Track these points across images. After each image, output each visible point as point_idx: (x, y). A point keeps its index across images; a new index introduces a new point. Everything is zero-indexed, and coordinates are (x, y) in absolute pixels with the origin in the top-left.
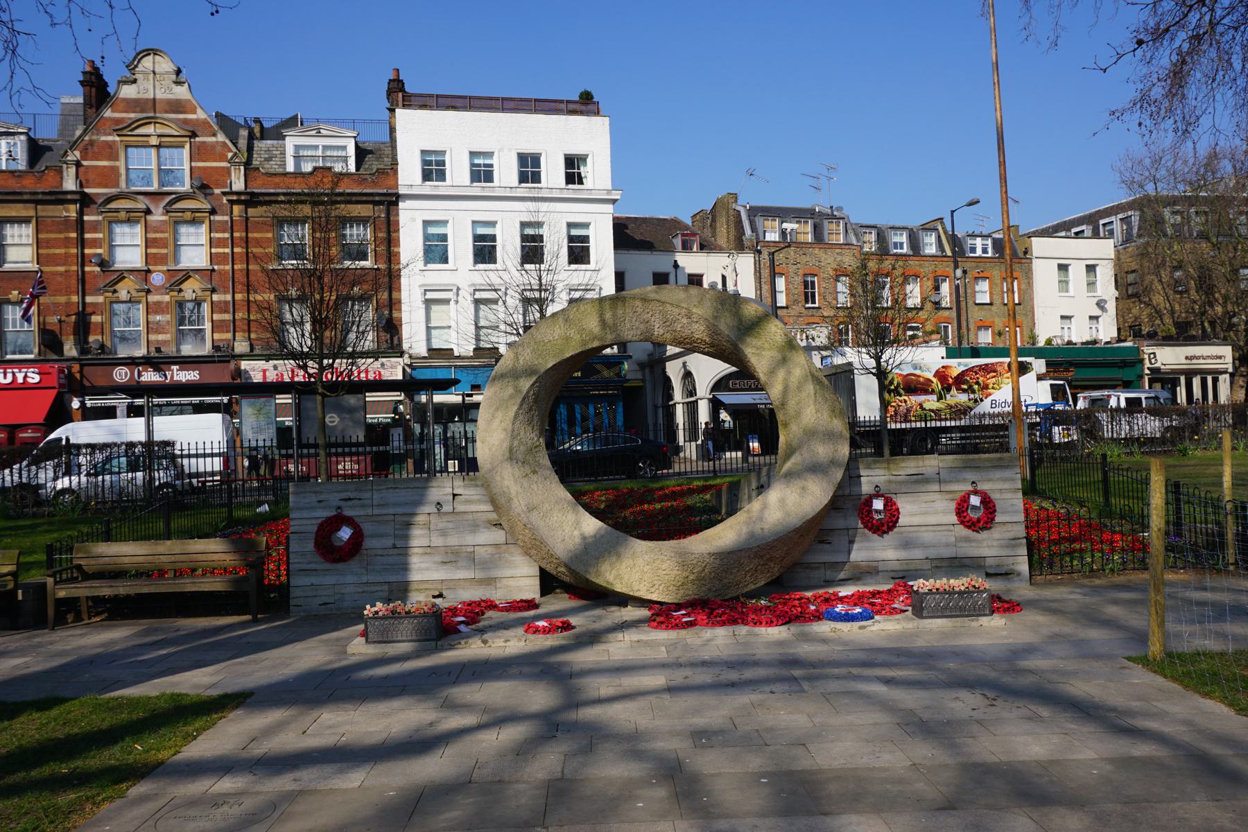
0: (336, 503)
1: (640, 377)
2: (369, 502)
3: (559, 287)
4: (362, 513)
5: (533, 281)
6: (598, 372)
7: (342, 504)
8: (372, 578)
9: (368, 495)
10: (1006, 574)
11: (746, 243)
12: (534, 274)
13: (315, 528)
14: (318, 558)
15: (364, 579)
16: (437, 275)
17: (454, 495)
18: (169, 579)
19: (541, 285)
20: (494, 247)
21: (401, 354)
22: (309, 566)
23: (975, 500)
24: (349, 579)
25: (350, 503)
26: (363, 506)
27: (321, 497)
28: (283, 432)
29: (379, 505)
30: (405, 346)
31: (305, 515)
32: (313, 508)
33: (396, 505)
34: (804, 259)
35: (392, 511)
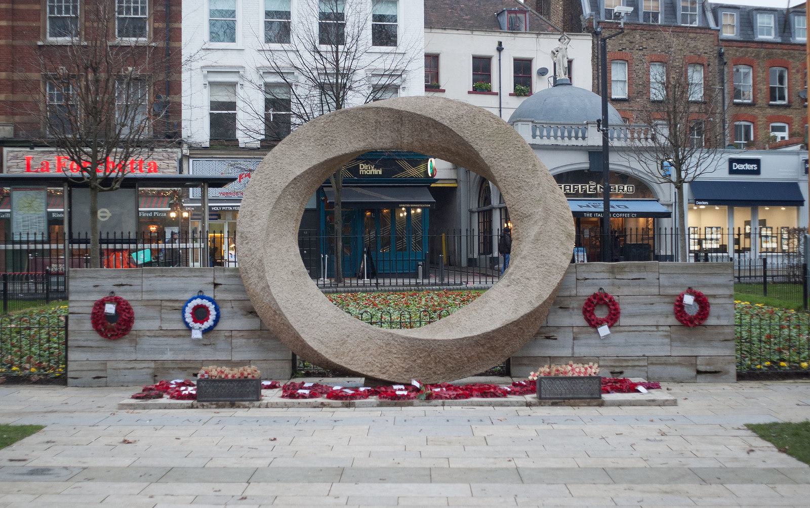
0: (110, 288)
1: (454, 177)
2: (139, 288)
3: (360, 75)
4: (133, 298)
5: (328, 66)
6: (402, 170)
7: (115, 289)
8: (140, 357)
9: (138, 282)
10: (716, 372)
11: (584, 24)
12: (330, 56)
13: (90, 310)
14: (97, 336)
15: (133, 357)
16: (224, 56)
17: (216, 285)
18: (303, 396)
19: (338, 70)
20: (234, 22)
21: (180, 144)
22: (85, 344)
23: (689, 300)
24: (120, 356)
25: (122, 288)
26: (133, 292)
27: (97, 282)
28: (53, 221)
29: (147, 291)
30: (185, 134)
31: (82, 298)
32: (89, 292)
33: (163, 291)
34: (651, 44)
35: (159, 297)
